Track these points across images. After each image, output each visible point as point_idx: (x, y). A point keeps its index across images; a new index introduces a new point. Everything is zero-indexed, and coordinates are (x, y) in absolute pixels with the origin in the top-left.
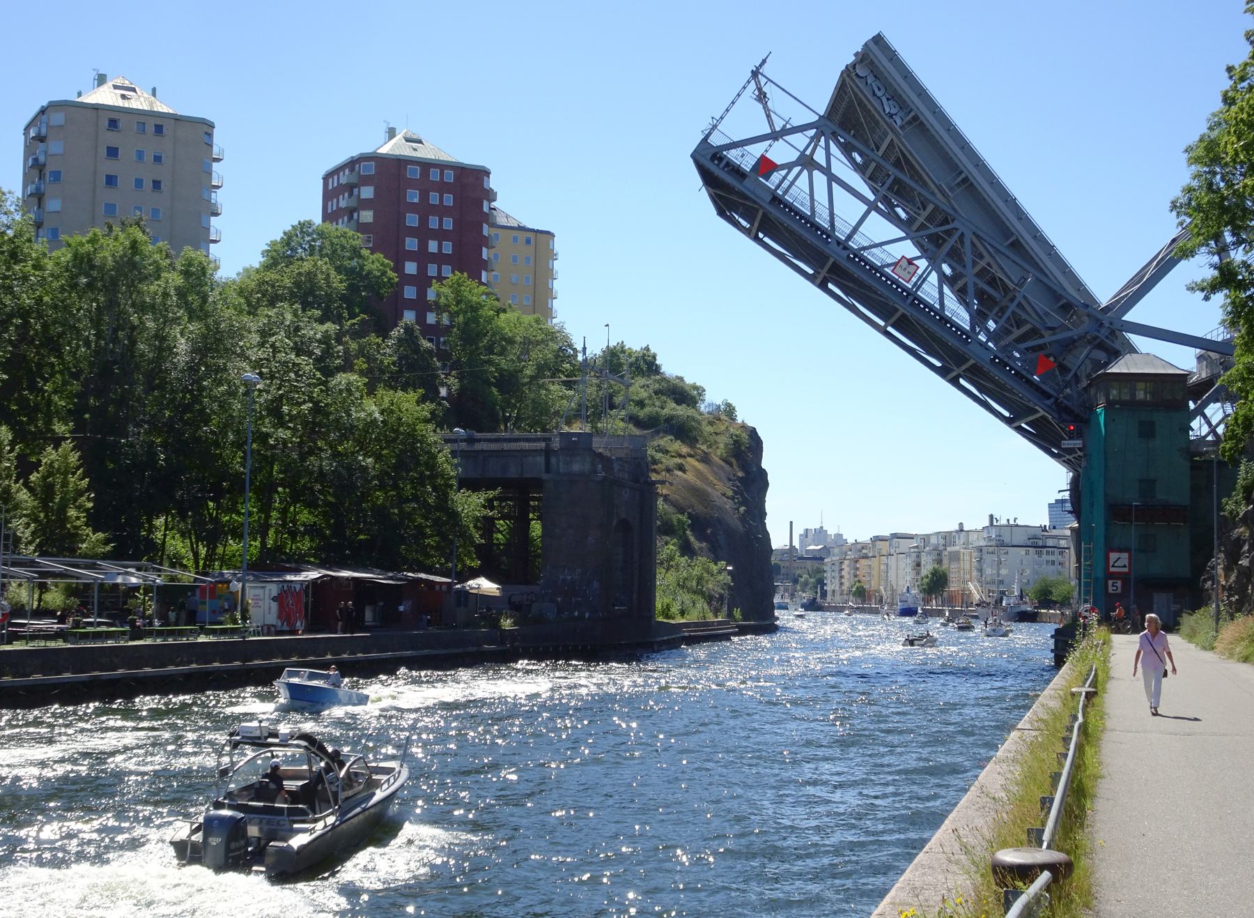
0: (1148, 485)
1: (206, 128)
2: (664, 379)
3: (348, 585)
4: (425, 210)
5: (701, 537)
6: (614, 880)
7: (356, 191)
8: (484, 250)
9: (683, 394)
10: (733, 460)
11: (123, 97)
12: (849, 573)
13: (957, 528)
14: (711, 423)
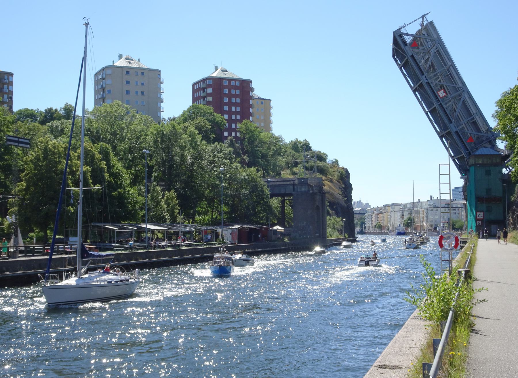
0: (488, 190)
1: (158, 73)
2: (314, 152)
3: (247, 229)
4: (230, 96)
5: (332, 209)
7: (205, 90)
8: (251, 109)
9: (321, 157)
10: (340, 181)
11: (129, 62)
12: (375, 219)
13: (85, 26)
14: (331, 168)
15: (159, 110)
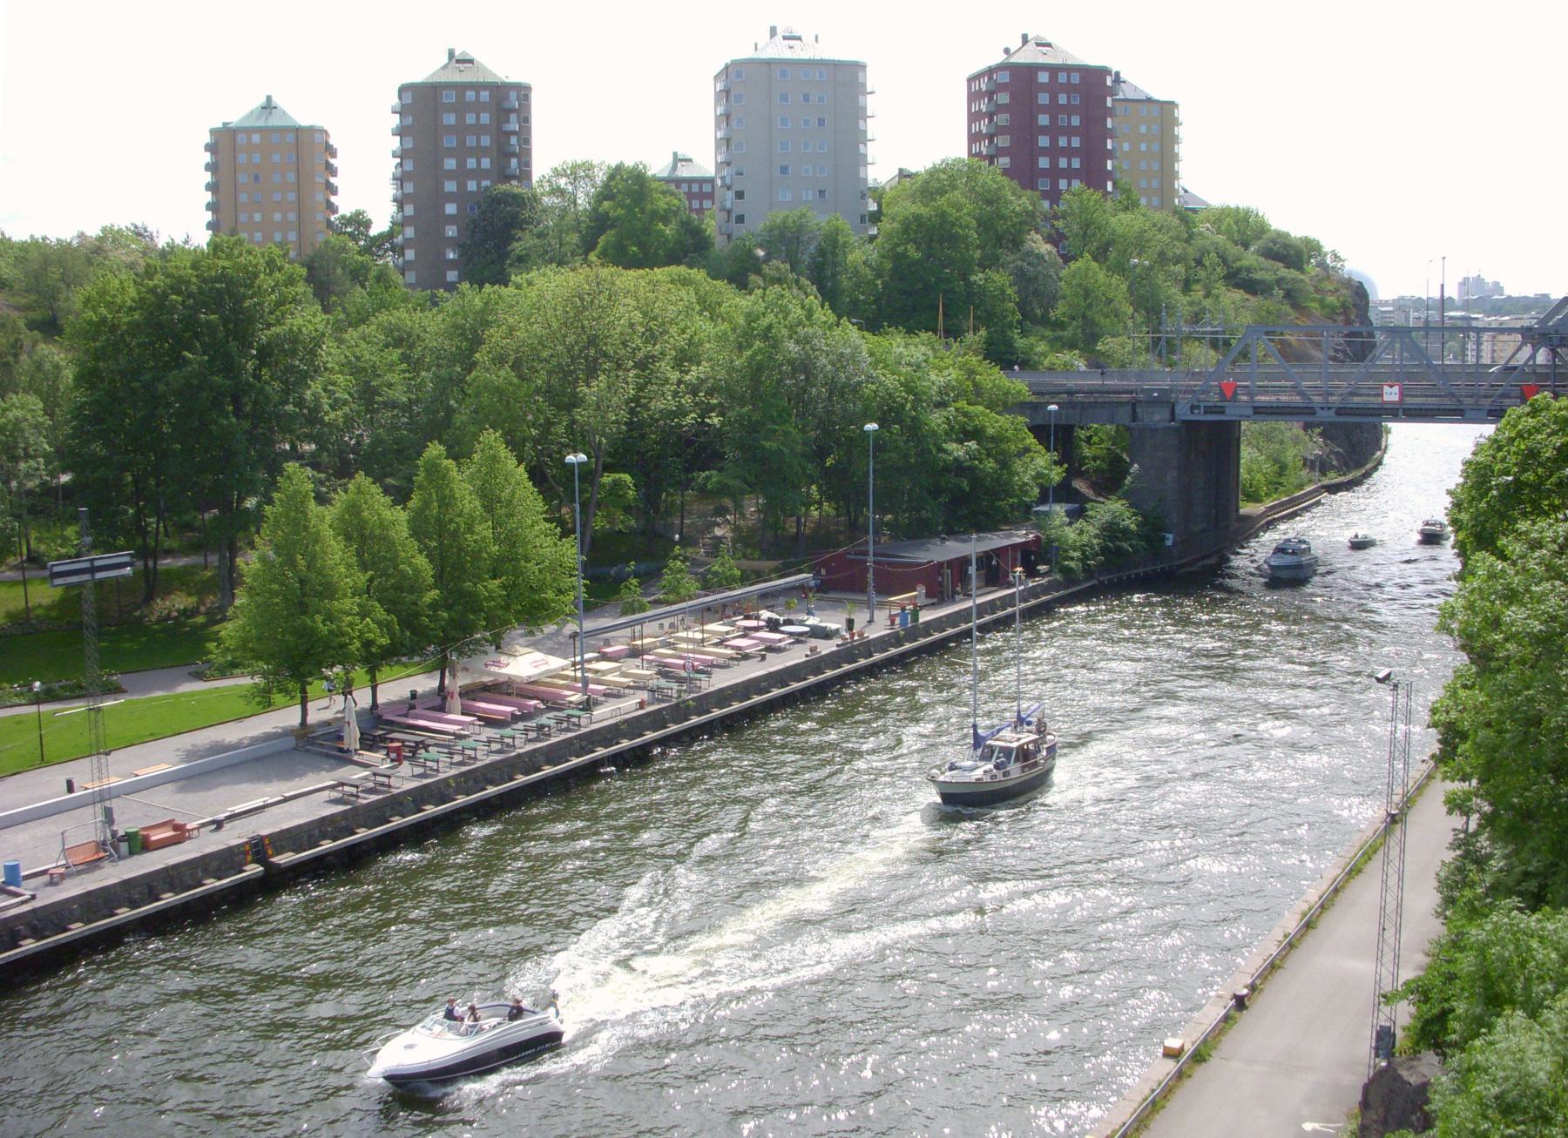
6: (1379, 392)
8: (1109, 141)
15: (861, 160)
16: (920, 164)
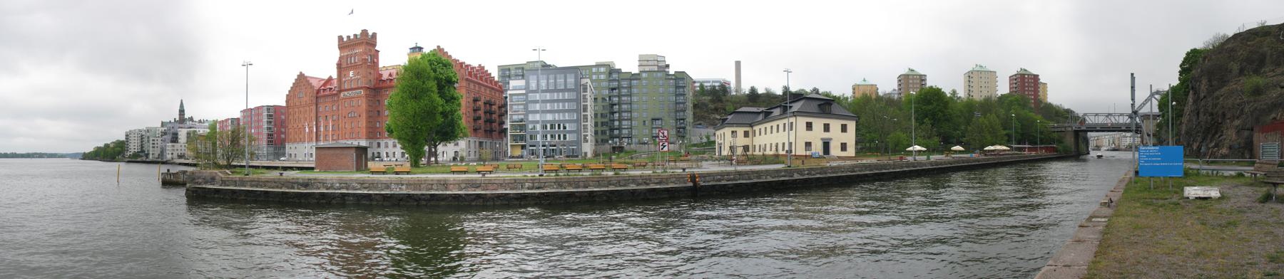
16: (1003, 93)
